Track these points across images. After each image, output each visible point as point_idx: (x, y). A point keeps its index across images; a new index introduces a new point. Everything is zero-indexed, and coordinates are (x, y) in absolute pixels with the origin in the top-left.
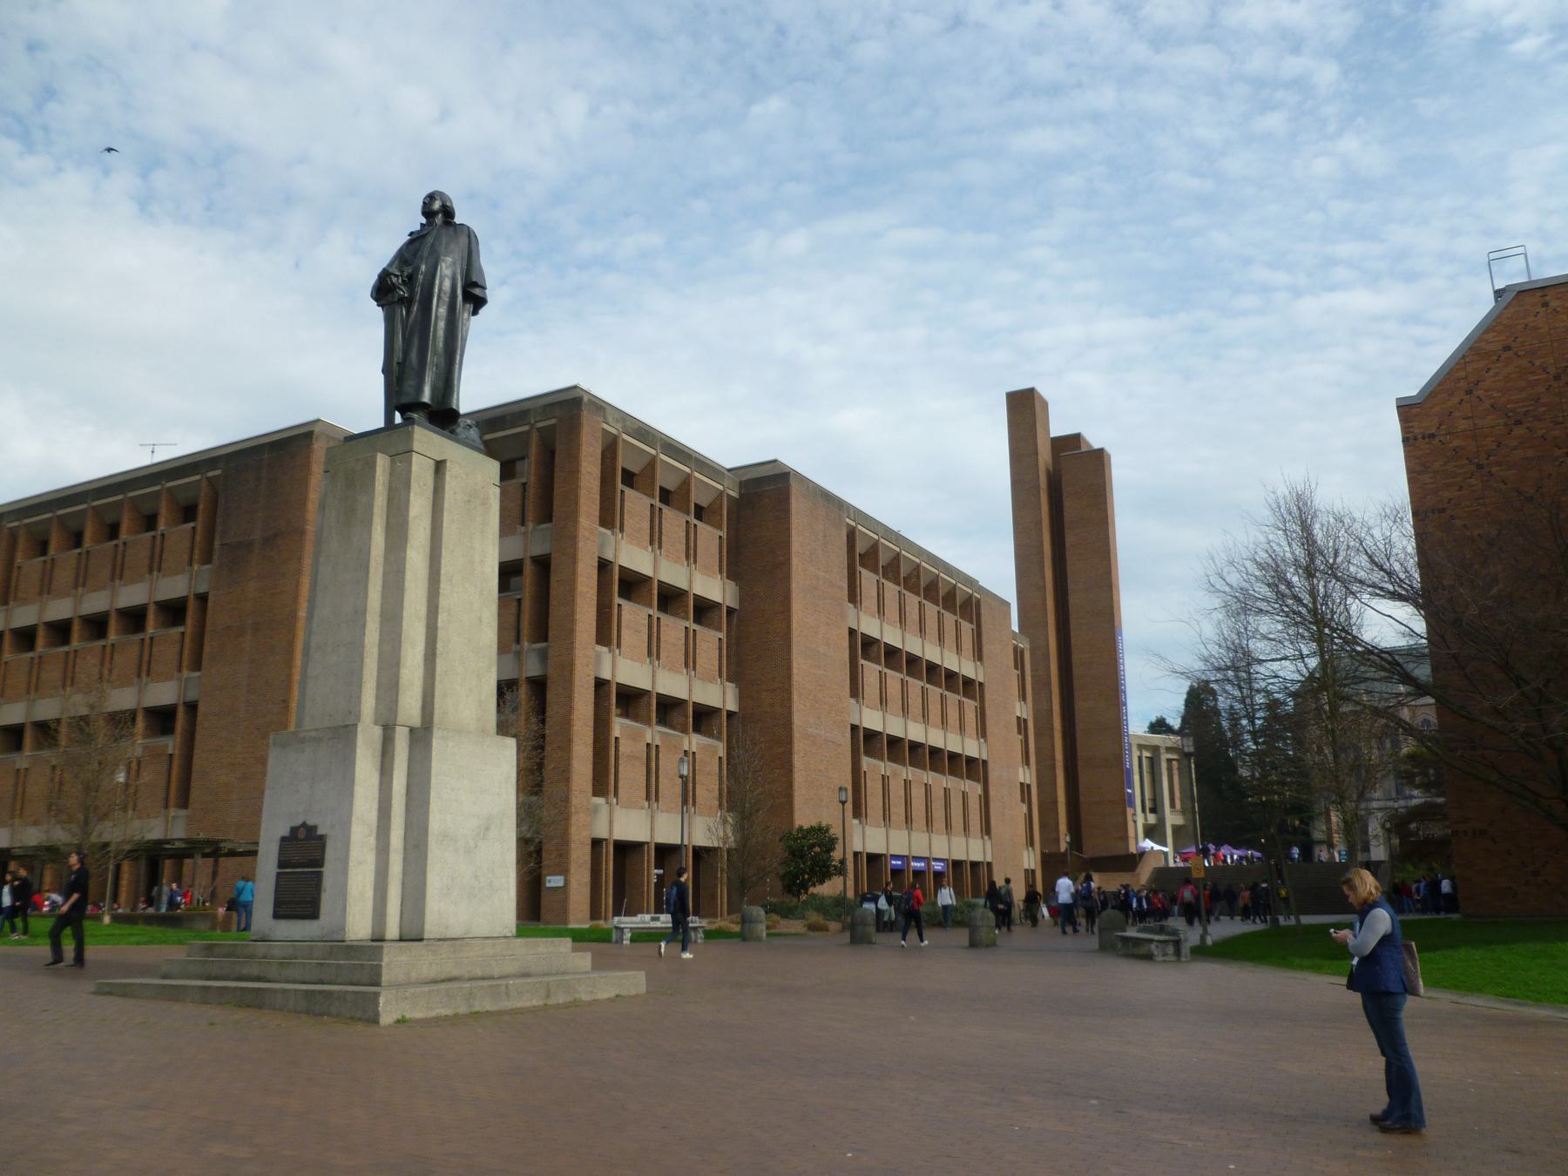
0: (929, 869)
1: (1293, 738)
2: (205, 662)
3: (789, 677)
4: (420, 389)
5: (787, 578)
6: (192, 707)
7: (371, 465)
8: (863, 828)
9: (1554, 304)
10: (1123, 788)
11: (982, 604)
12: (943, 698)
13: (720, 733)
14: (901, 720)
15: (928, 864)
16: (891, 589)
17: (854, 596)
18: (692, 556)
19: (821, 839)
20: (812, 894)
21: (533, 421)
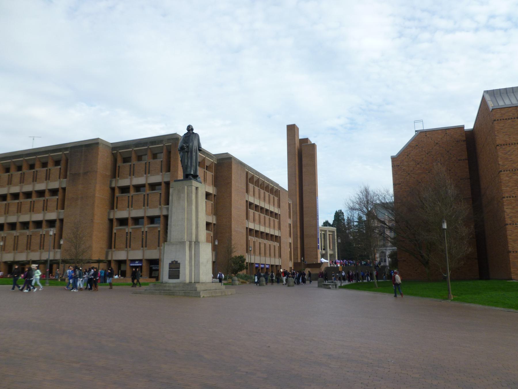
2: (65, 208)
3: (231, 215)
5: (231, 187)
6: (62, 221)
7: (184, 188)
9: (428, 136)
10: (317, 244)
11: (280, 192)
12: (274, 221)
13: (212, 230)
14: (269, 229)
16: (257, 188)
17: (247, 191)
20: (239, 274)
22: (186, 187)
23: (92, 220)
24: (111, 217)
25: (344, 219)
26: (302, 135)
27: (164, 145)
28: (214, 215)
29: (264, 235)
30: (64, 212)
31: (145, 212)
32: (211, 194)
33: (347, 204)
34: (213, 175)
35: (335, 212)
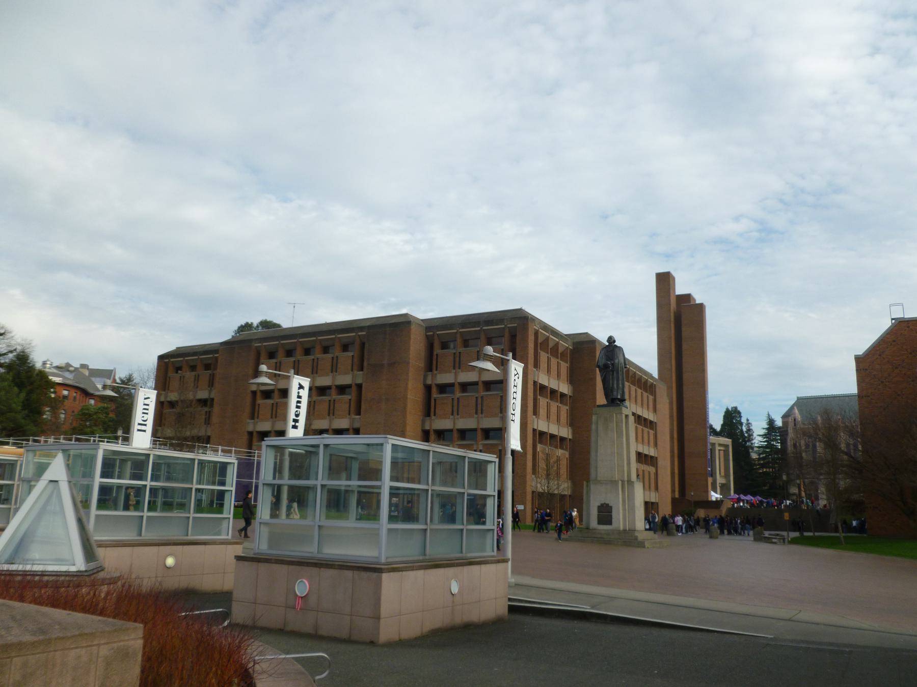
1: (780, 440)
2: (362, 413)
8: (650, 493)
12: (643, 430)
13: (567, 448)
22: (615, 415)
23: (402, 431)
24: (427, 428)
26: (680, 289)
27: (506, 326)
28: (570, 426)
31: (478, 423)
35: (725, 410)
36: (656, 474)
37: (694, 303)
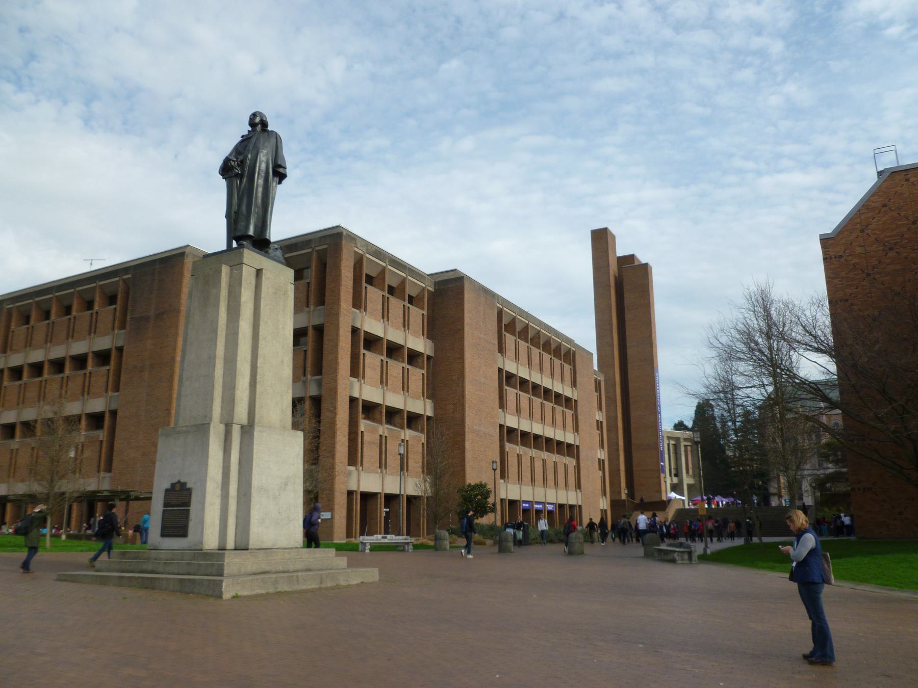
0: (545, 509)
3: (463, 397)
4: (247, 228)
6: (114, 413)
9: (912, 179)
13: (423, 429)
15: (544, 506)
16: (523, 345)
17: (501, 349)
18: (407, 325)
19: (482, 491)
21: (313, 246)
23: (167, 410)
25: (715, 417)
27: (313, 249)
29: (542, 441)
30: (118, 396)
32: (420, 355)
33: (713, 340)
34: (426, 314)
36: (578, 468)
37: (639, 264)
